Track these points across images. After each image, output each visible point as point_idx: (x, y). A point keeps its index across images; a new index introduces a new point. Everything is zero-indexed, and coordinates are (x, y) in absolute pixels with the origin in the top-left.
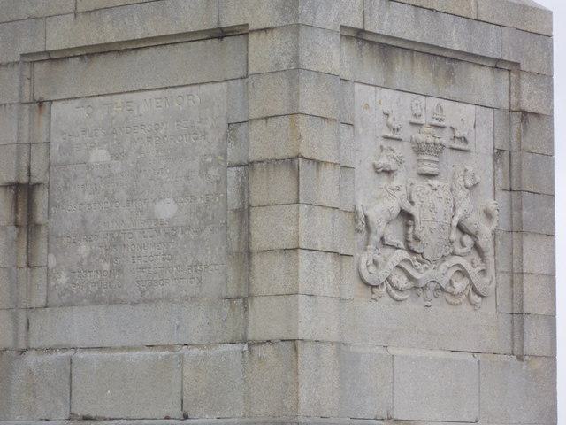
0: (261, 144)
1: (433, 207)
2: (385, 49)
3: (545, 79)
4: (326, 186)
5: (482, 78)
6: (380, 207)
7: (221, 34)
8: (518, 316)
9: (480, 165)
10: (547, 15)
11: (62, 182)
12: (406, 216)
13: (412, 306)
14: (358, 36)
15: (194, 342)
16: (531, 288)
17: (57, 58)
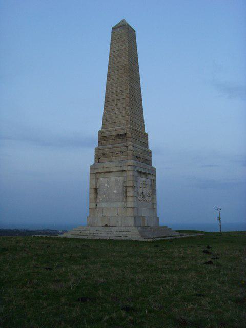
7: (123, 171)
17: (101, 173)
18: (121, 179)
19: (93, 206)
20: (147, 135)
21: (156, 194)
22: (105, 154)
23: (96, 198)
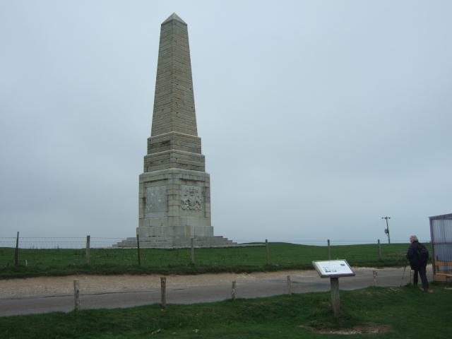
0: (170, 192)
1: (193, 199)
2: (186, 180)
3: (209, 183)
4: (177, 197)
5: (200, 183)
6: (185, 200)
7: (165, 179)
8: (205, 212)
9: (200, 194)
10: (209, 175)
11: (60, 328)
12: (188, 201)
13: (190, 212)
14: (182, 179)
15: (317, 275)
16: (207, 209)
17: (148, 182)
18: (164, 188)
19: (142, 216)
20: (200, 139)
21: (210, 202)
22: (151, 163)
23: (144, 208)
